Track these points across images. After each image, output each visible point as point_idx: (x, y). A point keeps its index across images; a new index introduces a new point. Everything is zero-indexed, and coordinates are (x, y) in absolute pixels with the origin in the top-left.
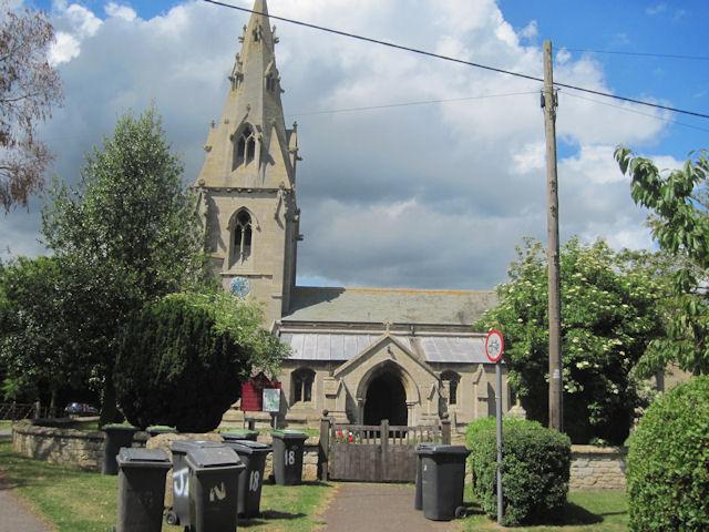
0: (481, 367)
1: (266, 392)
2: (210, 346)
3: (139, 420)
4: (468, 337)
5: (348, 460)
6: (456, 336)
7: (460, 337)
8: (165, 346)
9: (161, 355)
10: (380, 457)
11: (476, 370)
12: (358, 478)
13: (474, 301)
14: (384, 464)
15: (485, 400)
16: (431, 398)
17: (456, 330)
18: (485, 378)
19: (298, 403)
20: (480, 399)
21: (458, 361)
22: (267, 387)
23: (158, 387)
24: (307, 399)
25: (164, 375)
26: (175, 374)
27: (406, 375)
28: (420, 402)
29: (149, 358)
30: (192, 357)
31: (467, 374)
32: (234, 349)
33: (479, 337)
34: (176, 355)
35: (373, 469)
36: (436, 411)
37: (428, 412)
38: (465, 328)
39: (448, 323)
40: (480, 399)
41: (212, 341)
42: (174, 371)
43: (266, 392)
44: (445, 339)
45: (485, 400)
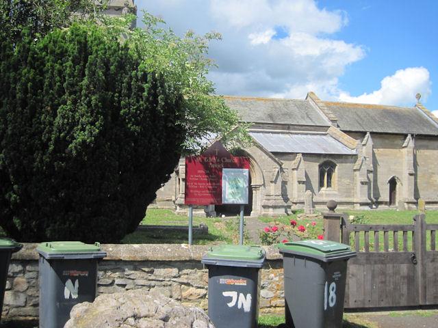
0: (300, 156)
1: (227, 173)
2: (139, 97)
3: (16, 221)
4: (278, 133)
5: (369, 277)
6: (269, 132)
7: (272, 133)
8: (61, 92)
9: (55, 108)
10: (414, 270)
11: (294, 159)
12: (383, 305)
13: (277, 106)
14: (420, 280)
15: (303, 183)
16: (275, 182)
17: (268, 128)
18: (303, 165)
19: (323, 189)
20: (299, 182)
21: (323, 152)
22: (227, 166)
23: (50, 166)
24: (329, 185)
25: (62, 143)
26: (84, 141)
27: (253, 161)
28: (264, 185)
29: (33, 116)
30: (109, 111)
31: (288, 162)
32: (176, 106)
33: (287, 133)
34: (83, 108)
35: (404, 289)
36: (280, 192)
37: (272, 193)
38: (276, 125)
39: (263, 122)
40: (299, 182)
41: (143, 90)
42: (80, 136)
43: (227, 173)
44: (261, 134)
45: (303, 183)
